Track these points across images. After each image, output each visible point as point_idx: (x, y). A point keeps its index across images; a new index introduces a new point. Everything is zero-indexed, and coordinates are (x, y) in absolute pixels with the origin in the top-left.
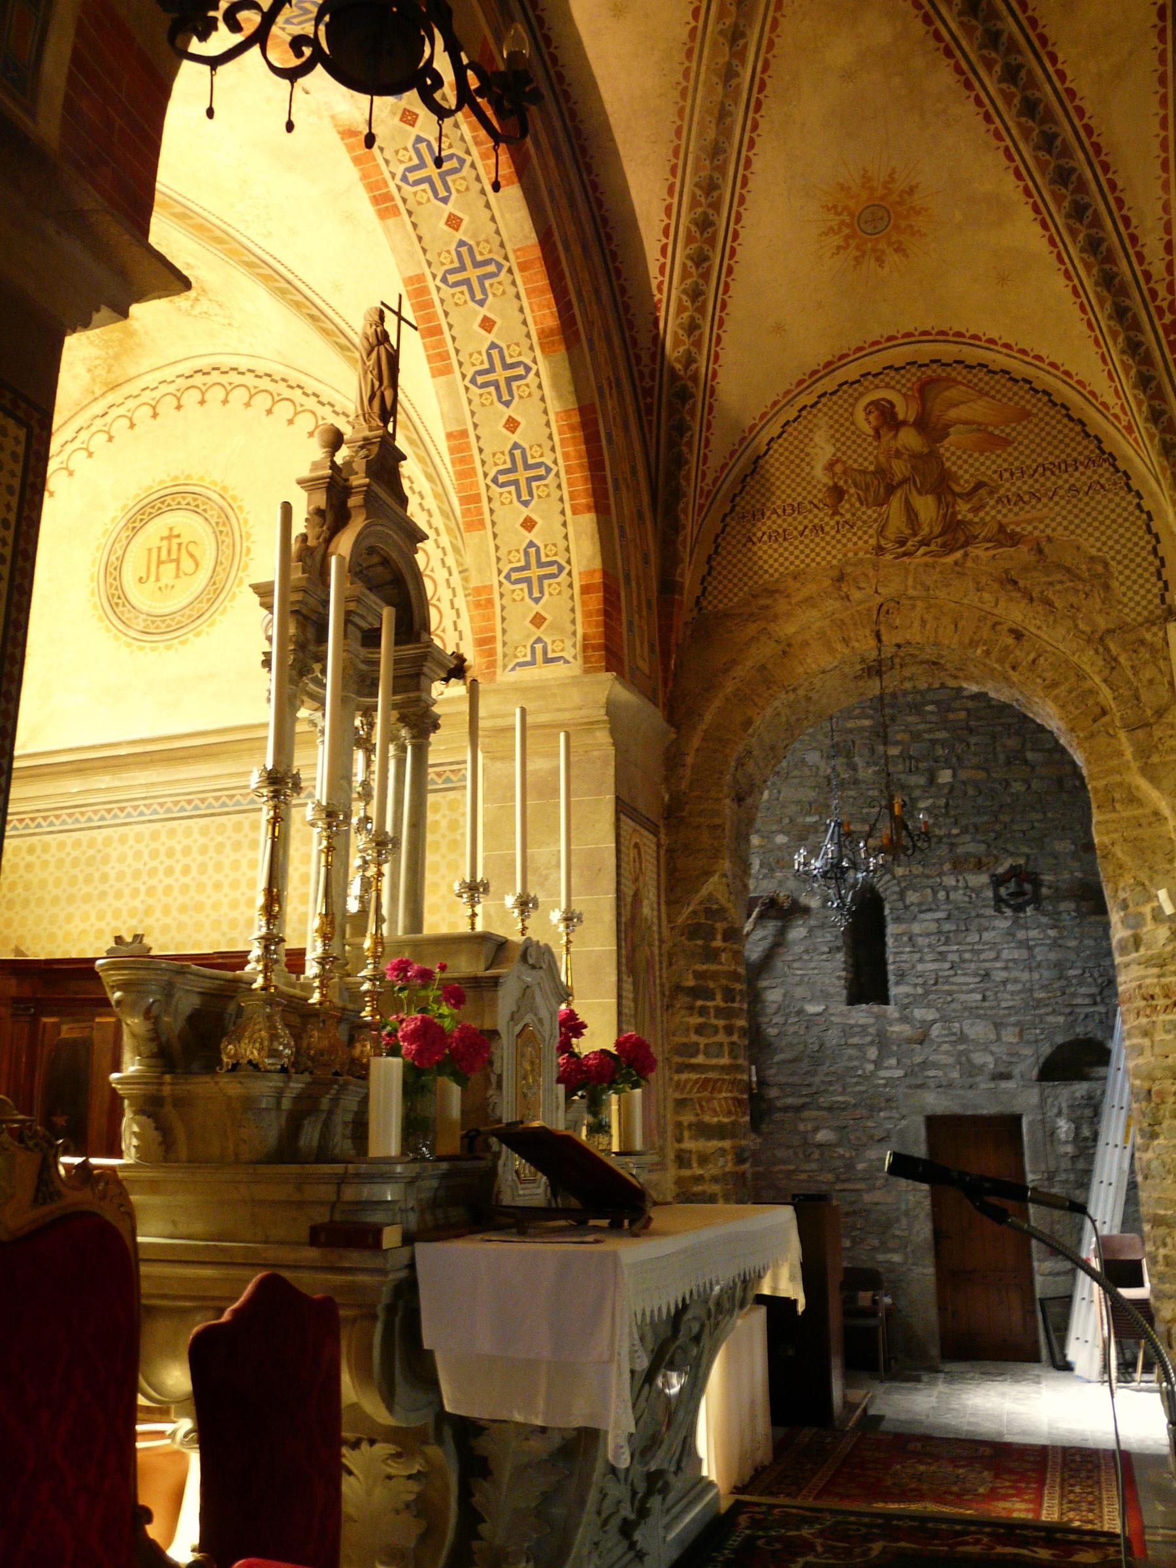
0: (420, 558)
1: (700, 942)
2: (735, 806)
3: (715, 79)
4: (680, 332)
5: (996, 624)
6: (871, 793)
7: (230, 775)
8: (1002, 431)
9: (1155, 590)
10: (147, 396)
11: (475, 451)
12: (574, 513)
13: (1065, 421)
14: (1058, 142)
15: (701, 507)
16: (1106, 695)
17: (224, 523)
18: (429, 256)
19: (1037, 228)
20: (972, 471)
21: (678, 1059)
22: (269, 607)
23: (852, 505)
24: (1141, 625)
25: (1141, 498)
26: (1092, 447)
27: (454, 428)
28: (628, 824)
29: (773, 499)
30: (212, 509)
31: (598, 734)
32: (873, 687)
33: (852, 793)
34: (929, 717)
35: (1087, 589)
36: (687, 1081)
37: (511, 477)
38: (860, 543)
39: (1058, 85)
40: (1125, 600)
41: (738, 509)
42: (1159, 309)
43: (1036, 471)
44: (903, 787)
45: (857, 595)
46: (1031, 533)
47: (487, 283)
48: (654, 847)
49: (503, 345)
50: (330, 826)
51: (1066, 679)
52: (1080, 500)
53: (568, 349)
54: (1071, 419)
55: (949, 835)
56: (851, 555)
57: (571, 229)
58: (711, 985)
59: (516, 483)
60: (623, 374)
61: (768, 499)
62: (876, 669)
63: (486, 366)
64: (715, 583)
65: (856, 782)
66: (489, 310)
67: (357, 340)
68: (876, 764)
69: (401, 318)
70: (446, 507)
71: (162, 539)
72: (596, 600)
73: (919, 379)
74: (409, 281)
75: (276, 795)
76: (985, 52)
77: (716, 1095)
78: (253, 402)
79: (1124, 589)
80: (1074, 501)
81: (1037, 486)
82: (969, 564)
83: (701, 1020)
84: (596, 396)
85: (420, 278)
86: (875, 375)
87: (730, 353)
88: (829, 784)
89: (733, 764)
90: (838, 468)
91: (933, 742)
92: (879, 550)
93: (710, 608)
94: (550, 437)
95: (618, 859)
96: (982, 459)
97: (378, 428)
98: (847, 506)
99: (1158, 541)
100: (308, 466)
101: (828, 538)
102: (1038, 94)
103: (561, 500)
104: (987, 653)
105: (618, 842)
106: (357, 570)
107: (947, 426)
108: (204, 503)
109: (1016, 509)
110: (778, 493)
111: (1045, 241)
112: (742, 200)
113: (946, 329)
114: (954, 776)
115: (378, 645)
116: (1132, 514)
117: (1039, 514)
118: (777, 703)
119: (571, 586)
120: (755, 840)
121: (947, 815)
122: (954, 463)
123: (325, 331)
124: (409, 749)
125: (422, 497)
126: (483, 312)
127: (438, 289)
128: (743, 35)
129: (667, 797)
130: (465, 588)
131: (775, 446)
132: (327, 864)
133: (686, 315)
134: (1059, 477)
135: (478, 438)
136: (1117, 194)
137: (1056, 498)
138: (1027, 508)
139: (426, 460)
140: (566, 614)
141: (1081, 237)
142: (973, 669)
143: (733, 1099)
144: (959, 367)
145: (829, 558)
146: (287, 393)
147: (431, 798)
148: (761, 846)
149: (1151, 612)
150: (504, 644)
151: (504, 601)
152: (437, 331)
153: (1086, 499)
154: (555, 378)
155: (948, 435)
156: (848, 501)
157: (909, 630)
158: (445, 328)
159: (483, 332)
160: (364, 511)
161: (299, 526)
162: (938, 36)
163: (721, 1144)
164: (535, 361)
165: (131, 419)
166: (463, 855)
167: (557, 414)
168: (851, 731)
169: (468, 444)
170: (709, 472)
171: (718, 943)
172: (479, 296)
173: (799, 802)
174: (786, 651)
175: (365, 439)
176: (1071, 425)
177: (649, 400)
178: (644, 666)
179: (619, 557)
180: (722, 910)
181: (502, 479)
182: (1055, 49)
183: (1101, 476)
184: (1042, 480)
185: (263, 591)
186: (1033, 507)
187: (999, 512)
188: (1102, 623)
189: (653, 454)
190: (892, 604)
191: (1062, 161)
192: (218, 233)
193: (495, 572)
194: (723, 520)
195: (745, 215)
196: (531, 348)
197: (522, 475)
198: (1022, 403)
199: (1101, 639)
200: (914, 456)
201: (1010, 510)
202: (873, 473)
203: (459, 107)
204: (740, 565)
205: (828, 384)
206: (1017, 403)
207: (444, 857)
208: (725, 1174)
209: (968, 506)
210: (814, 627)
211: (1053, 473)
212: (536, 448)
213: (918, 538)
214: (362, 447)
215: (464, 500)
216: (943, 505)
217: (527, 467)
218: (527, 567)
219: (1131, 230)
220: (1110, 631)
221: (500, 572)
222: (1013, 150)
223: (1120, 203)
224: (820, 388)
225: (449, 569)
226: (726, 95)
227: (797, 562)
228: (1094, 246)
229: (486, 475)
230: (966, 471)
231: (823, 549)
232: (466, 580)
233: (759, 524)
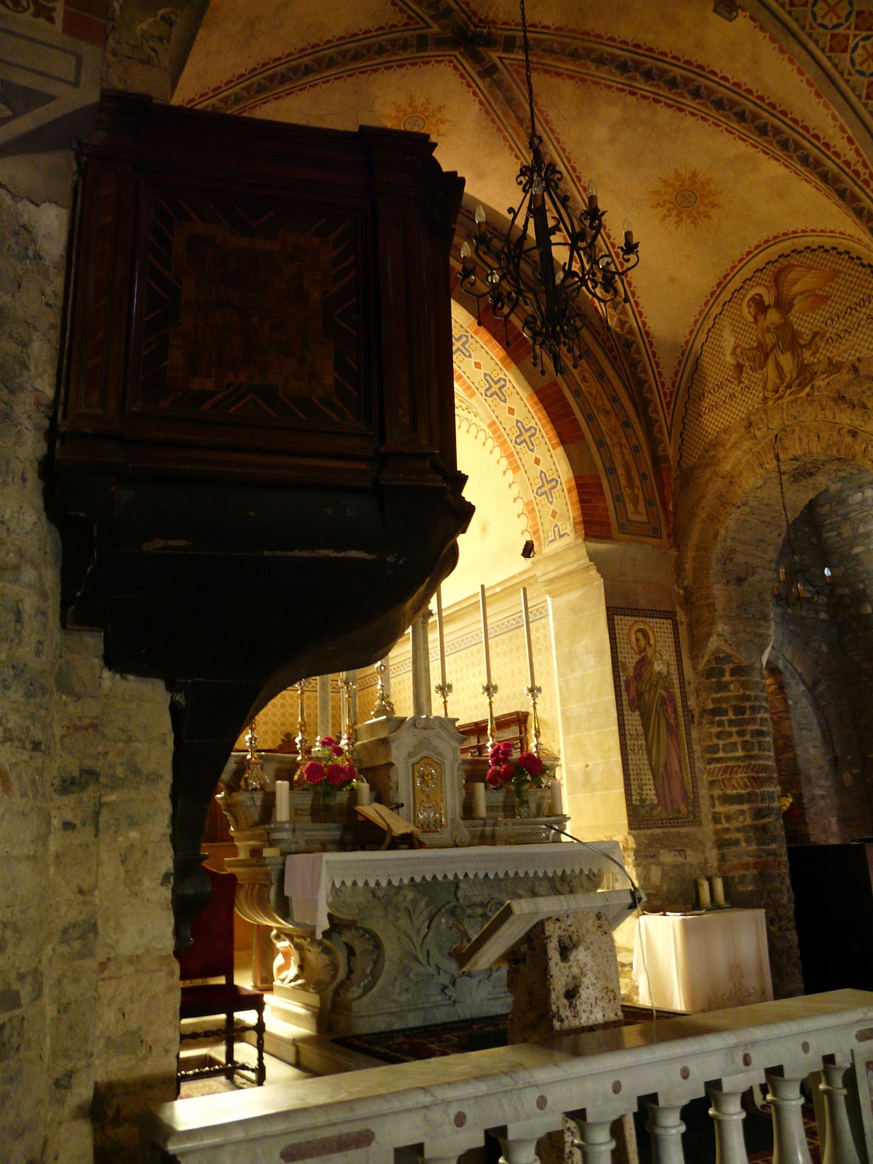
1: (714, 680)
8: (824, 291)
12: (554, 449)
15: (668, 404)
19: (775, 162)
21: (708, 756)
23: (748, 374)
27: (489, 422)
36: (715, 768)
37: (522, 438)
39: (727, 84)
42: (866, 182)
45: (759, 434)
49: (489, 373)
53: (516, 363)
56: (751, 408)
58: (724, 706)
59: (525, 441)
77: (734, 776)
83: (720, 729)
90: (739, 350)
94: (529, 412)
101: (738, 401)
102: (719, 96)
119: (563, 491)
126: (473, 360)
129: (682, 592)
136: (801, 124)
137: (860, 329)
138: (844, 341)
143: (748, 778)
154: (517, 380)
155: (793, 305)
158: (462, 374)
162: (644, 97)
163: (740, 807)
171: (727, 678)
174: (731, 480)
176: (864, 270)
180: (730, 656)
182: (711, 68)
184: (850, 318)
189: (627, 383)
190: (783, 433)
202: (757, 348)
205: (725, 296)
206: (830, 267)
208: (744, 827)
209: (810, 352)
211: (856, 311)
213: (785, 385)
218: (543, 486)
219: (822, 141)
223: (805, 128)
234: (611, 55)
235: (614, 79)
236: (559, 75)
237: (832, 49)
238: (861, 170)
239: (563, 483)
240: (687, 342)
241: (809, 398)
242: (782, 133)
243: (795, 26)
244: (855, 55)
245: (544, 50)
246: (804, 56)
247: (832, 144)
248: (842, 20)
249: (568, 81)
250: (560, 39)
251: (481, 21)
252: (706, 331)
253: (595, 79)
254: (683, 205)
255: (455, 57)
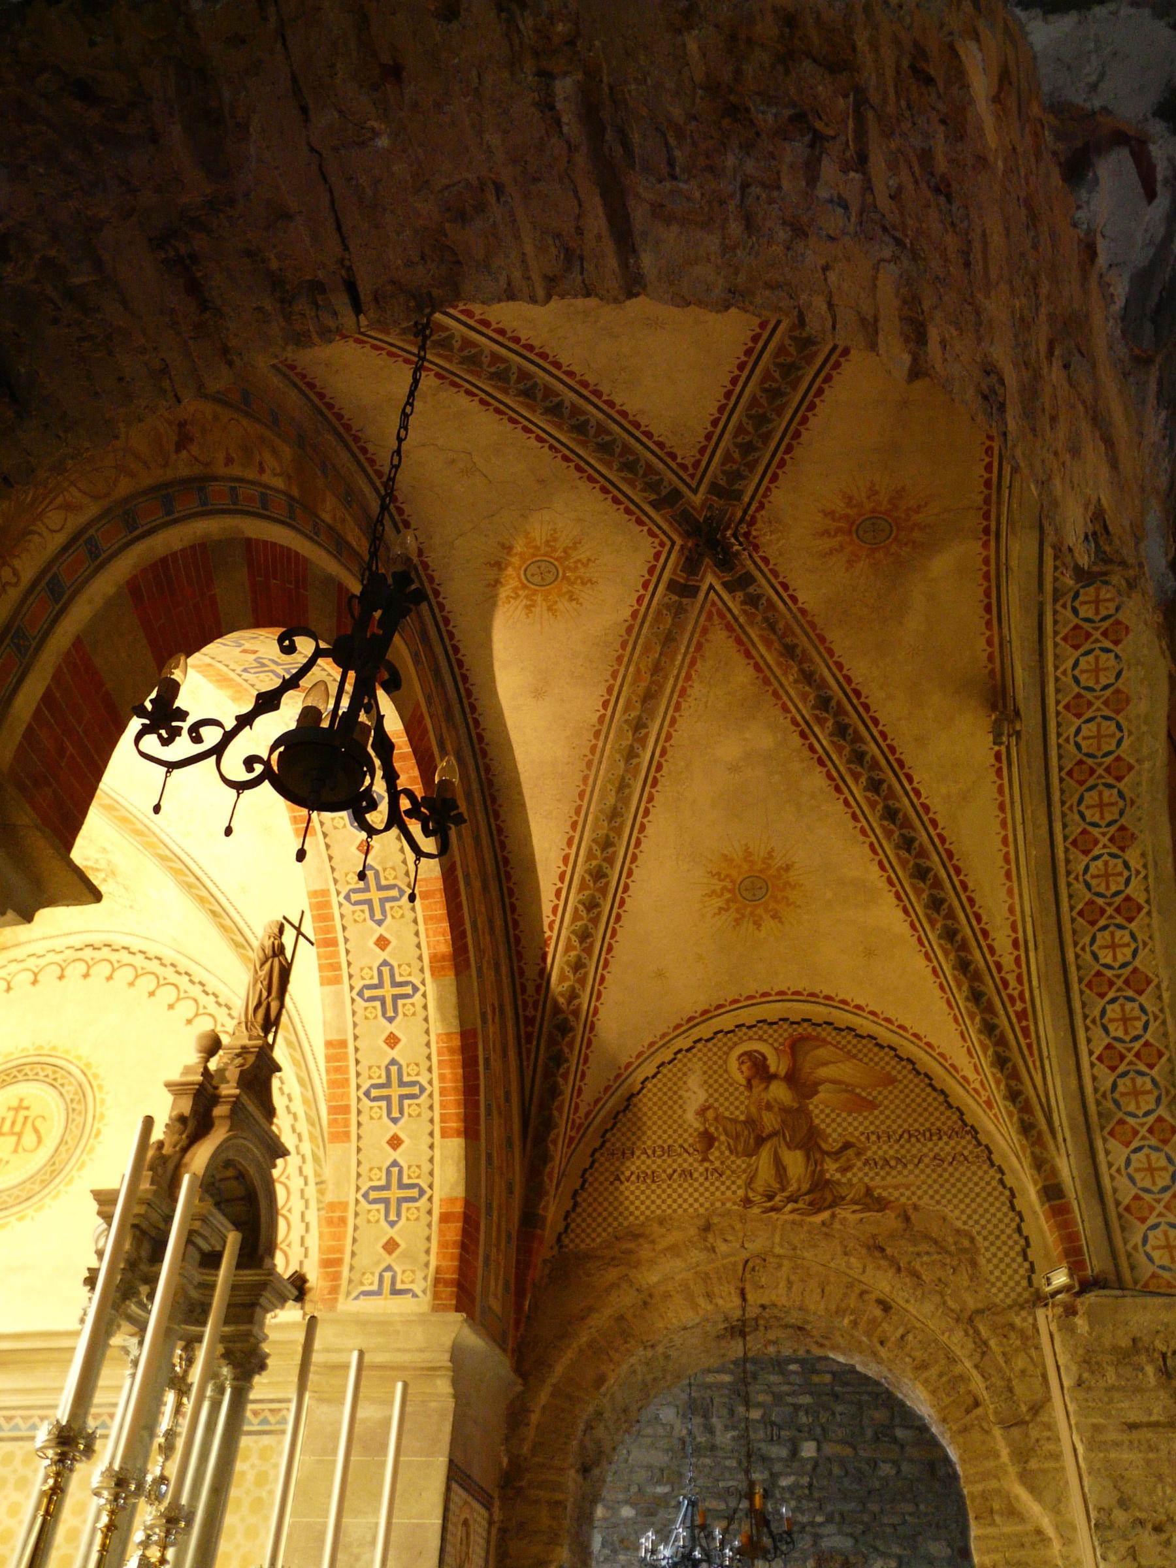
0: (275, 1173)
2: (579, 1478)
3: (618, 757)
4: (567, 969)
5: (862, 1293)
6: (728, 1463)
7: (16, 1391)
9: (1022, 1271)
10: (31, 963)
11: (352, 1063)
12: (444, 1135)
13: (929, 1090)
14: (916, 844)
15: (572, 1139)
16: (978, 1384)
17: (79, 1098)
18: (336, 875)
20: (840, 1130)
22: (107, 1218)
23: (722, 1153)
24: (1010, 1307)
25: (1003, 1173)
26: (955, 1118)
27: (335, 1037)
28: (459, 1492)
29: (644, 1138)
30: (70, 1083)
31: (439, 1382)
32: (736, 1348)
33: (708, 1461)
34: (793, 1378)
35: (955, 1263)
37: (384, 1092)
38: (729, 1193)
39: (915, 800)
40: (993, 1279)
41: (608, 1145)
43: (901, 1136)
44: (764, 1459)
45: (722, 1248)
46: (897, 1199)
47: (388, 905)
48: (485, 1524)
50: (116, 1497)
51: (936, 1361)
52: (945, 1170)
53: (457, 974)
54: (934, 1089)
55: (812, 1524)
56: (718, 1204)
57: (473, 866)
59: (388, 1098)
60: (508, 1001)
61: (639, 1138)
62: (739, 1330)
63: (375, 981)
64: (579, 1220)
65: (713, 1448)
66: (387, 930)
67: (256, 944)
68: (734, 1428)
69: (299, 933)
70: (313, 1114)
71: (9, 1109)
72: (454, 1230)
73: (791, 1035)
74: (313, 894)
75: (62, 1459)
76: (852, 766)
78: (138, 982)
79: (987, 1244)
80: (939, 1170)
81: (903, 1151)
82: (837, 1226)
84: (479, 1020)
85: (325, 893)
86: (749, 1027)
87: (613, 994)
88: (684, 1448)
89: (582, 1426)
90: (710, 1114)
91: (796, 1407)
92: (747, 1202)
93: (571, 1246)
94: (429, 1058)
95: (443, 1539)
96: (850, 1119)
97: (259, 1037)
98: (717, 1153)
99: (1022, 1220)
100: (180, 1069)
101: (696, 1185)
103: (432, 1121)
104: (855, 1323)
105: (445, 1519)
106: (209, 1186)
107: (817, 1084)
108: (63, 1077)
109: (882, 1173)
110: (649, 1133)
111: (907, 924)
112: (634, 858)
113: (817, 991)
114: (819, 1449)
115: (217, 1266)
116: (995, 1189)
117: (904, 1181)
118: (633, 1360)
119: (430, 1212)
120: (600, 1512)
121: (810, 1497)
122: (823, 1121)
123: (223, 927)
124: (228, 1392)
125: (290, 1100)
126: (380, 931)
127: (340, 905)
128: (645, 726)
129: (505, 1461)
130: (319, 1201)
131: (650, 1086)
132: (104, 1547)
133: (573, 953)
134: (924, 1145)
135: (357, 1050)
137: (921, 1166)
138: (894, 1173)
139: (301, 1063)
140: (420, 1243)
141: (938, 926)
142: (841, 1340)
144: (829, 1028)
145: (696, 1205)
146: (173, 978)
147: (245, 1442)
148: (605, 1519)
149: (1020, 1295)
150: (352, 1268)
151: (358, 1221)
152: (333, 943)
153: (951, 1169)
154: (440, 1000)
155: (816, 1092)
156: (718, 1148)
157: (774, 1291)
158: (341, 940)
159: (377, 950)
160: (228, 1123)
161: (158, 1134)
162: (812, 749)
164: (423, 983)
165: (9, 983)
166: (266, 1518)
167: (438, 1035)
168: (709, 1386)
169: (346, 1054)
170: (581, 1105)
172: (378, 916)
173: (649, 1467)
175: (243, 1047)
176: (934, 1094)
177: (530, 1029)
178: (495, 1305)
179: (483, 1184)
181: (374, 1093)
183: (964, 1148)
184: (908, 1146)
185: (105, 1200)
186: (900, 1173)
187: (866, 1175)
188: (972, 1304)
189: (528, 1081)
191: (920, 861)
192: (140, 826)
193: (353, 1188)
194: (592, 1155)
195: (636, 871)
196: (422, 970)
197: (395, 1092)
198: (888, 1068)
199: (971, 1320)
200: (784, 1110)
201: (877, 1174)
202: (744, 1122)
203: (387, 828)
204: (606, 1194)
205: (704, 1031)
207: (243, 1520)
210: (677, 1278)
212: (413, 1066)
213: (786, 1194)
214: (238, 1055)
215: (333, 1110)
216: (812, 1161)
217: (402, 1084)
218: (386, 1187)
220: (978, 1312)
221: (358, 1189)
222: (877, 846)
223: (971, 901)
224: (696, 1033)
225: (306, 1178)
226: (626, 771)
227: (664, 1207)
228: (950, 934)
229: (358, 1087)
230: (834, 1130)
231: (691, 1195)
232: (321, 1192)
233: (628, 1163)
234: (823, 679)
235: (800, 706)
236: (748, 655)
237: (1074, 843)
238: (1013, 983)
239: (436, 1200)
240: (629, 1064)
241: (824, 1229)
242: (942, 889)
243: (1056, 796)
244: (1093, 865)
245: (766, 619)
246: (1044, 831)
247: (992, 935)
248: (1103, 823)
249: (751, 669)
250: (792, 621)
251: (747, 535)
252: (658, 1062)
253: (781, 691)
254: (745, 894)
255: (673, 543)
